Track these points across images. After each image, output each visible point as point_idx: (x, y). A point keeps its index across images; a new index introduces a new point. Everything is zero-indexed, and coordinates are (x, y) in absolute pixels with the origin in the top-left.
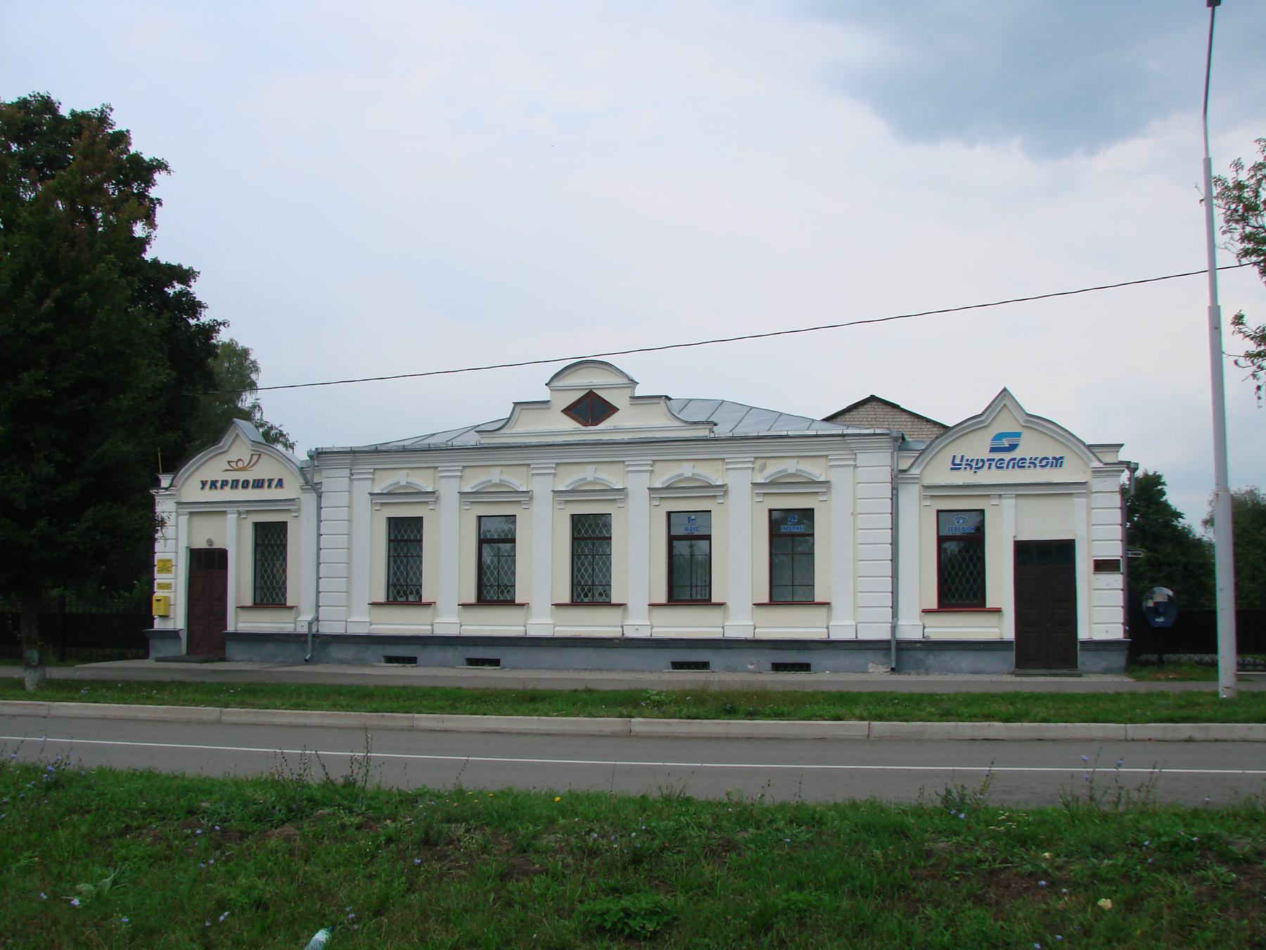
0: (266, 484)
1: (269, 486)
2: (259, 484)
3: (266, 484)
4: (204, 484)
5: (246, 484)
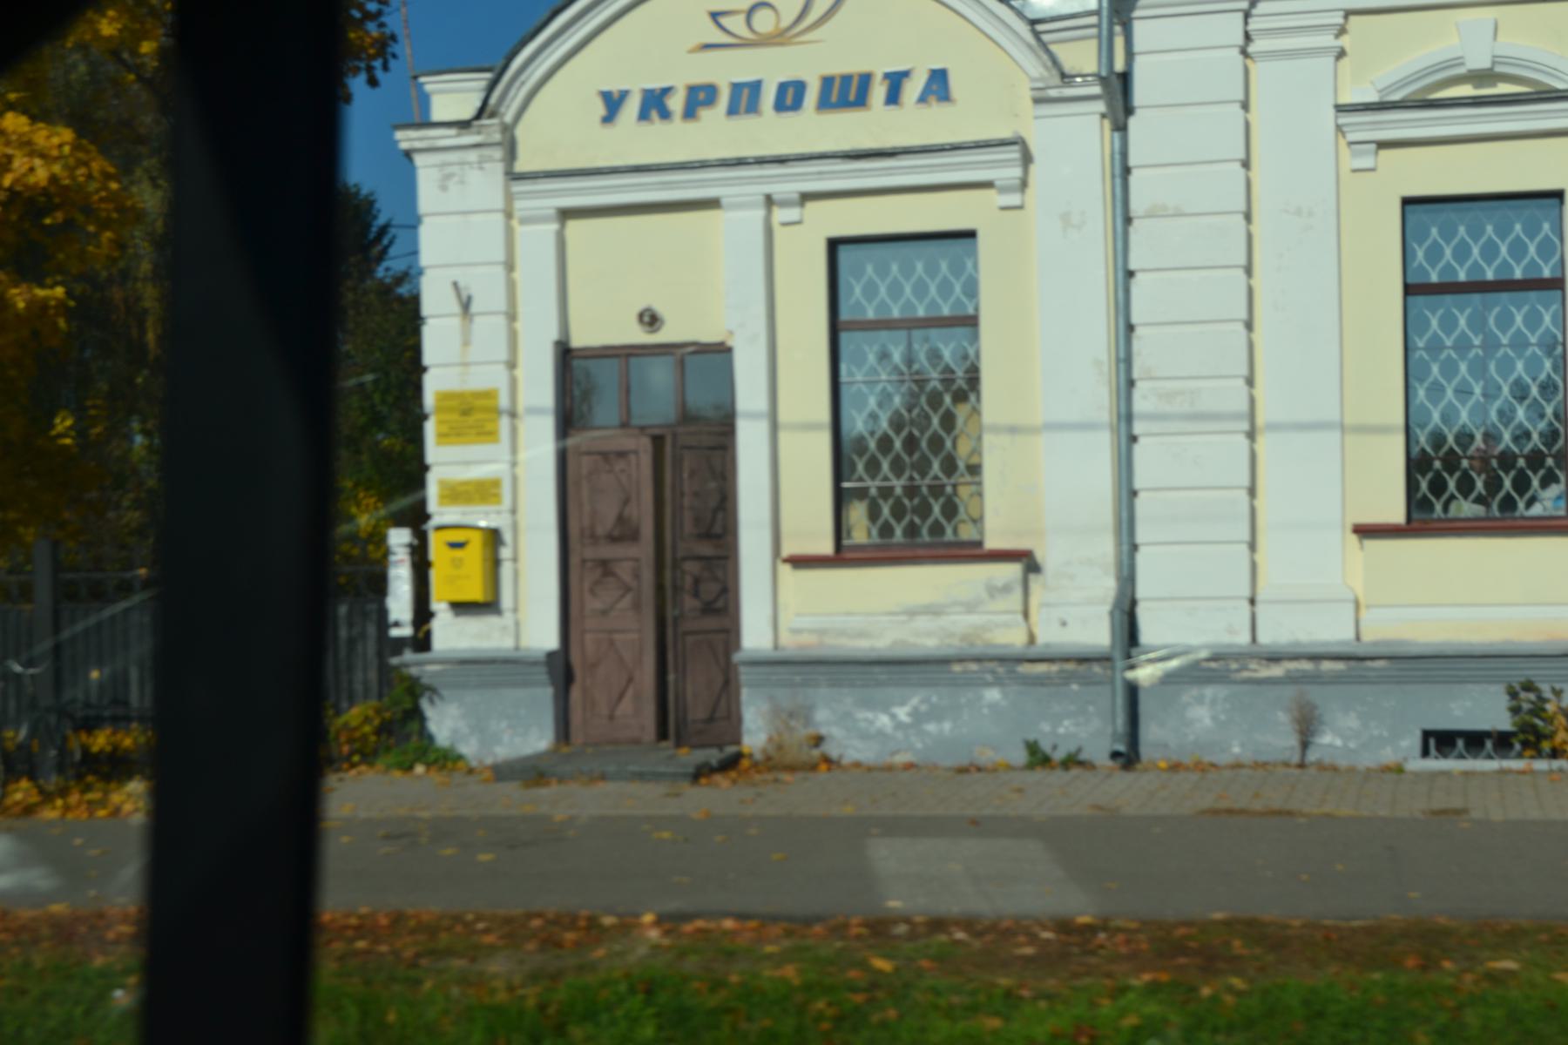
0: (879, 92)
1: (893, 98)
2: (846, 93)
3: (879, 92)
4: (613, 103)
5: (790, 97)
